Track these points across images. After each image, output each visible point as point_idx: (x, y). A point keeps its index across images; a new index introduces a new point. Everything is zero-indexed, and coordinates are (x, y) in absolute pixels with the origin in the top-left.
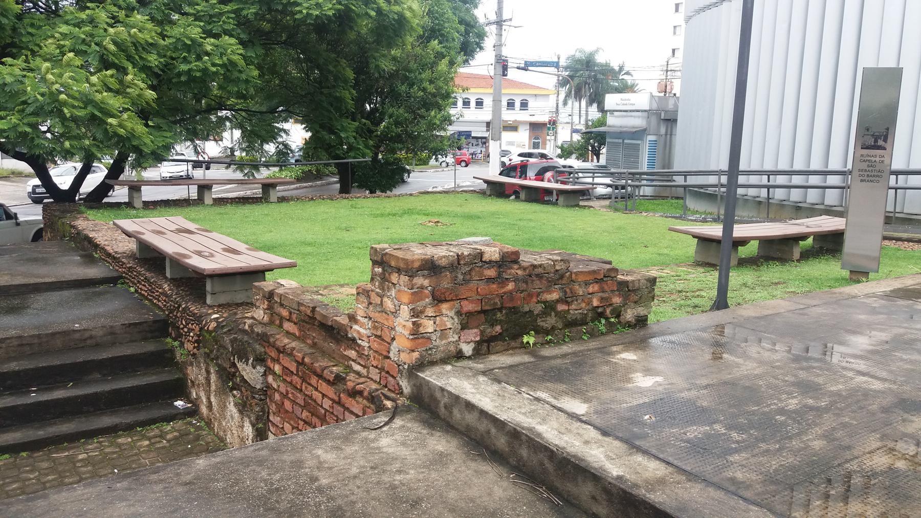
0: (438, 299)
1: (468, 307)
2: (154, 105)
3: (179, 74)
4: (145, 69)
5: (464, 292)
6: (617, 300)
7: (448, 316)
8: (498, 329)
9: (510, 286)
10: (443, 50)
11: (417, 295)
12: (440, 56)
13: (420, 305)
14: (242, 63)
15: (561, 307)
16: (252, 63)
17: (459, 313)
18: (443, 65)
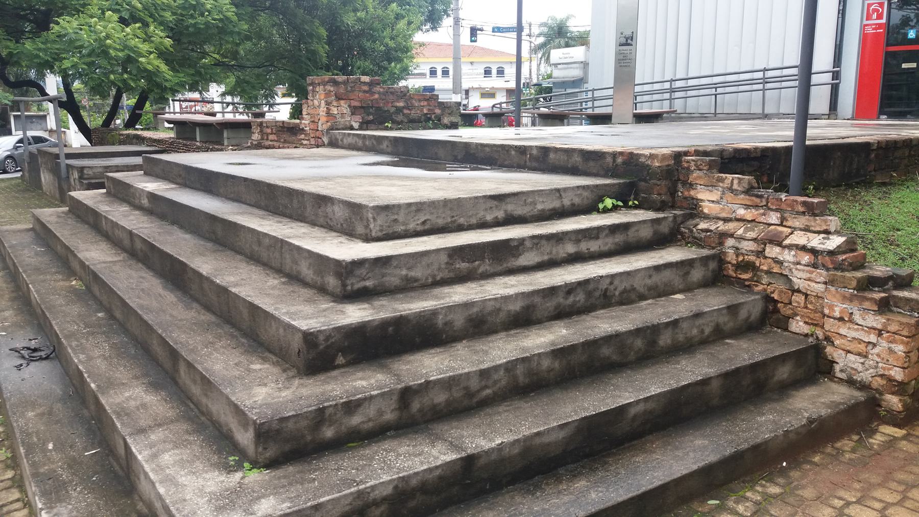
0: (339, 98)
1: (357, 104)
2: (171, 49)
3: (188, 27)
4: (162, 23)
5: (352, 96)
6: (438, 111)
7: (344, 107)
8: (371, 117)
9: (376, 96)
10: (403, 12)
11: (328, 94)
12: (398, 17)
13: (330, 99)
14: (235, 18)
15: (406, 111)
16: (243, 20)
17: (349, 106)
18: (402, 24)
